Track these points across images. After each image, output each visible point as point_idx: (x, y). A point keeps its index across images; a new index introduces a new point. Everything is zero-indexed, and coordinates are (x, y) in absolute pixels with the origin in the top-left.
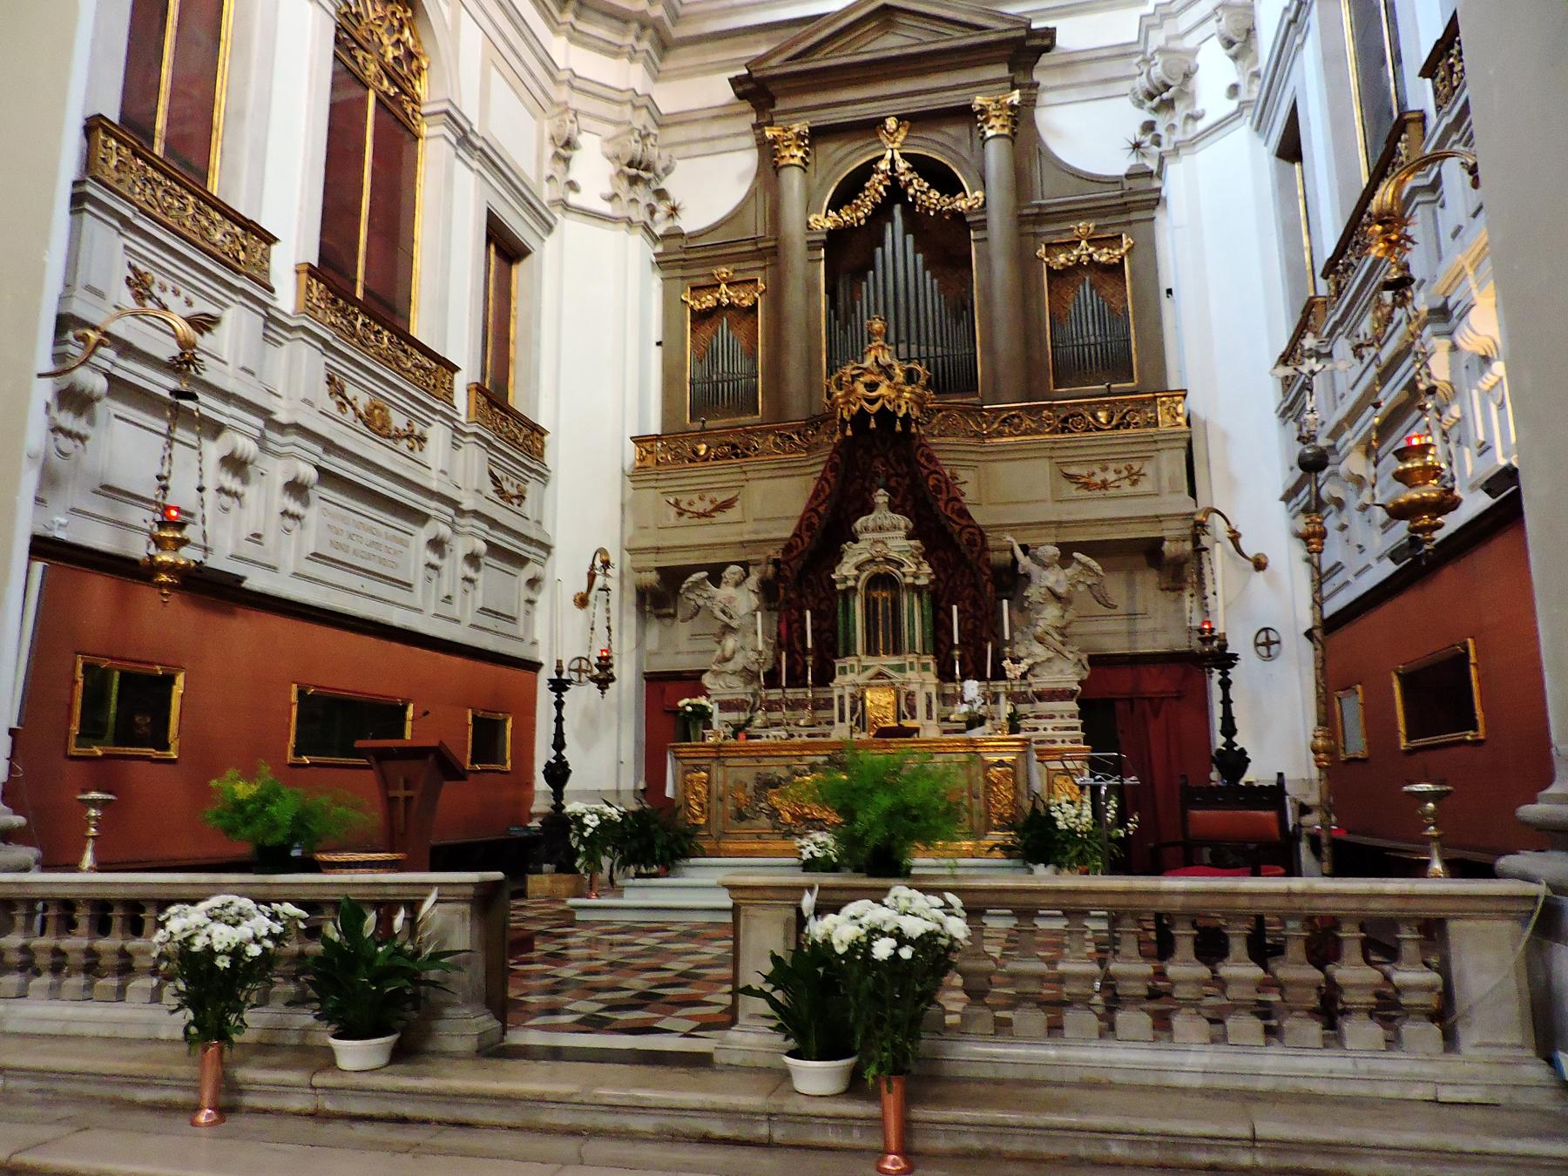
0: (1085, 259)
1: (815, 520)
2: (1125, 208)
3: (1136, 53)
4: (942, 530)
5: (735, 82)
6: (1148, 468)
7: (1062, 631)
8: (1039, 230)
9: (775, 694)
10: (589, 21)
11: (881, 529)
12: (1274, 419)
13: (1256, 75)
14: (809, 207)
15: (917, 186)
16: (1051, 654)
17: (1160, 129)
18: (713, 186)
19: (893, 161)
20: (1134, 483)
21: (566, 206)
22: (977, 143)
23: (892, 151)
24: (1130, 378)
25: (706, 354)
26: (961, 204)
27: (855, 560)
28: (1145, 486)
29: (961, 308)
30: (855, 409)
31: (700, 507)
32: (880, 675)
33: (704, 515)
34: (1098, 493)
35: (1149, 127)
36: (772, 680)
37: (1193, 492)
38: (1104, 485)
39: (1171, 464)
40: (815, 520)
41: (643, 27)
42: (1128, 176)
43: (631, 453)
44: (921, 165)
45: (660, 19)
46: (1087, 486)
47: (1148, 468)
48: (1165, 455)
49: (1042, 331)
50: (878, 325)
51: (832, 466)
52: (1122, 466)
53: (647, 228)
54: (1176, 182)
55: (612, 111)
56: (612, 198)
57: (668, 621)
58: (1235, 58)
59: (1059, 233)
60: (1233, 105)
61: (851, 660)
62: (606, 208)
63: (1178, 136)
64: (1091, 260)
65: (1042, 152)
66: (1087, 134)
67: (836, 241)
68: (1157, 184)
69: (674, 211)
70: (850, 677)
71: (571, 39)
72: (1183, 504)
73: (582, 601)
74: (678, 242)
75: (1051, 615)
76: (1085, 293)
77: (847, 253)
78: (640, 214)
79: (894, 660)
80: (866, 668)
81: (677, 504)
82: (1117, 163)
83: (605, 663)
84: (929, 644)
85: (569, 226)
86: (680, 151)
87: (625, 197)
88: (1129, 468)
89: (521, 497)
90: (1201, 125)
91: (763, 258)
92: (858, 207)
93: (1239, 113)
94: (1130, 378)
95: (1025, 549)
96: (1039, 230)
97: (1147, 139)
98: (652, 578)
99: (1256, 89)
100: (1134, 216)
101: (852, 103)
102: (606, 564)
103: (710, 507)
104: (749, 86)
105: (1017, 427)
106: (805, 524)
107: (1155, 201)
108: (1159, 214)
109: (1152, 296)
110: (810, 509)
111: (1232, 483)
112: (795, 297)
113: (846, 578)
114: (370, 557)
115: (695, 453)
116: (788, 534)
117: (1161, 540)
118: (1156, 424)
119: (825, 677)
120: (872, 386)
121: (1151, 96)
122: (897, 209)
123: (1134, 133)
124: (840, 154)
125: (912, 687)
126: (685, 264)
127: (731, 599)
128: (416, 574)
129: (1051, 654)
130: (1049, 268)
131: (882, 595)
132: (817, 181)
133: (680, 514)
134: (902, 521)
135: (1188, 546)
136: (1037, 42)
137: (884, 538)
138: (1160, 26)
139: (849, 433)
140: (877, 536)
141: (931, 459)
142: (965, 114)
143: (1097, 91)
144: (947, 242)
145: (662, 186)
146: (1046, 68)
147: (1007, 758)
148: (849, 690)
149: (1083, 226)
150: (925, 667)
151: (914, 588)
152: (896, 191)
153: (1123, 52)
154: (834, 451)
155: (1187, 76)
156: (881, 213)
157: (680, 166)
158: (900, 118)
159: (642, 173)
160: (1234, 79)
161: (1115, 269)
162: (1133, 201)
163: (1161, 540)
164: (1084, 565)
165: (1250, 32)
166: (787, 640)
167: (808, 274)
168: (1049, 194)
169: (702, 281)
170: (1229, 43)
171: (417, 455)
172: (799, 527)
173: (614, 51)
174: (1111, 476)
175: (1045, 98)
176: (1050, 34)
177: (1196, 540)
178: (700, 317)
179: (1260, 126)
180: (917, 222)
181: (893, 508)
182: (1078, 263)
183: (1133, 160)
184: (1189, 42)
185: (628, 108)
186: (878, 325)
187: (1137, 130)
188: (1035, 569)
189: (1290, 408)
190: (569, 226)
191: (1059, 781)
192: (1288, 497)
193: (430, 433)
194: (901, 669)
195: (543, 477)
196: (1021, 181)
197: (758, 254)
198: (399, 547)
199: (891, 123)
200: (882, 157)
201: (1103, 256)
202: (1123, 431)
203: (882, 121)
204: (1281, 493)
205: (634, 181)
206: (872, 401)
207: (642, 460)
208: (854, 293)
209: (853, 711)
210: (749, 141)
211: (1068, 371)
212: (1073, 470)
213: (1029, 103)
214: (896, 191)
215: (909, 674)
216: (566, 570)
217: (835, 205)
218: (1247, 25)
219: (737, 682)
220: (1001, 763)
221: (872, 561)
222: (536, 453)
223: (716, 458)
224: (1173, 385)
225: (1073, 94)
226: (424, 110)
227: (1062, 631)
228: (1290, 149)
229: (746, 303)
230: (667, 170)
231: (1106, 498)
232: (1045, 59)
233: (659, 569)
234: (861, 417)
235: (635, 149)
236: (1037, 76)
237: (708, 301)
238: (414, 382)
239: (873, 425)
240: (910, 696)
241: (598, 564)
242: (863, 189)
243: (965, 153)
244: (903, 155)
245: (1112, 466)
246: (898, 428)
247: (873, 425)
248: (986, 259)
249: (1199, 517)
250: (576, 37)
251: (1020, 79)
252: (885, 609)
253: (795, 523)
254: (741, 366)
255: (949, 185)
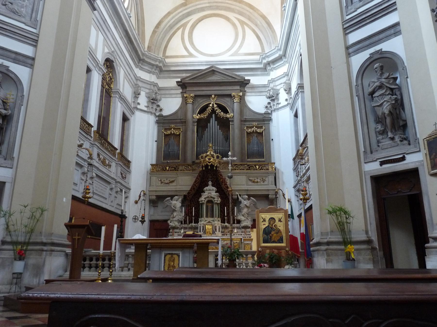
0: (255, 131)
1: (195, 187)
2: (264, 121)
3: (267, 87)
4: (223, 191)
5: (177, 82)
6: (267, 179)
7: (248, 214)
8: (245, 123)
9: (186, 226)
10: (144, 65)
11: (210, 190)
12: (292, 171)
13: (291, 98)
14: (193, 113)
15: (218, 111)
16: (245, 219)
17: (272, 105)
18: (171, 105)
19: (213, 105)
20: (264, 182)
21: (137, 109)
22: (232, 103)
23: (213, 102)
24: (264, 158)
25: (167, 145)
26: (228, 116)
27: (204, 197)
28: (266, 183)
29: (227, 138)
30: (205, 164)
31: (166, 182)
32: (209, 222)
33: (167, 183)
34: (256, 184)
35: (269, 103)
36: (185, 222)
37: (276, 185)
38: (257, 182)
39: (271, 178)
40: (195, 187)
41: (157, 67)
42: (264, 114)
43: (150, 167)
44: (220, 106)
45: (161, 66)
46: (254, 182)
47: (267, 179)
48: (270, 177)
49: (245, 146)
50: (211, 145)
51: (199, 175)
52: (261, 178)
53: (155, 114)
54: (274, 116)
55: (148, 87)
56: (147, 107)
57: (156, 208)
58: (287, 93)
59: (249, 124)
60: (286, 103)
61: (202, 219)
62: (146, 109)
63: (275, 107)
64: (256, 131)
65: (246, 106)
66: (256, 103)
67: (199, 120)
68: (270, 116)
69: (161, 110)
70: (202, 222)
71: (140, 69)
72: (273, 187)
73: (136, 202)
74: (162, 118)
75: (245, 210)
76: (254, 139)
77: (202, 125)
78: (154, 111)
79: (212, 219)
80: (206, 221)
81: (161, 180)
82: (262, 110)
83: (143, 217)
84: (219, 215)
85: (137, 113)
86: (163, 96)
87: (151, 107)
88: (263, 179)
89: (125, 178)
90: (280, 106)
91: (182, 123)
92: (205, 114)
93: (288, 104)
94: (264, 158)
95: (240, 195)
96: (245, 123)
97: (269, 106)
98: (154, 197)
99: (291, 100)
100: (266, 122)
101: (205, 91)
102: (145, 194)
103: (169, 182)
104: (181, 84)
105: (239, 168)
106: (193, 188)
107: (270, 120)
108: (270, 122)
109: (269, 140)
110: (194, 185)
111: (284, 183)
112: (189, 134)
113: (202, 201)
114: (99, 192)
115: (166, 169)
116: (189, 189)
117: (269, 195)
118: (268, 170)
119: (197, 222)
120: (210, 159)
121: (270, 98)
122: (214, 115)
123: (266, 104)
124: (201, 101)
125: (216, 225)
126: (163, 123)
127: (175, 204)
128: (107, 196)
129: (245, 219)
130: (247, 132)
131: (210, 205)
132: (196, 107)
133: (162, 183)
134: (215, 189)
135: (274, 196)
136: (246, 82)
137: (210, 192)
138: (272, 83)
139: (204, 169)
140: (209, 192)
141: (221, 175)
142: (230, 96)
143: (259, 94)
144: (225, 124)
145: (158, 104)
146: (248, 87)
147: (238, 242)
148: (202, 225)
149: (255, 124)
150: (219, 221)
151: (216, 203)
152: (213, 111)
153: (264, 86)
154: (200, 172)
155: (278, 94)
156: (210, 116)
157: (163, 99)
158: (215, 95)
159: (155, 102)
160: (287, 98)
161: (261, 134)
162: (265, 119)
163: (269, 195)
164: (253, 200)
165: (290, 89)
166: (188, 213)
167: (193, 129)
168: (247, 116)
169: (167, 127)
170: (286, 91)
171: (110, 169)
172: (191, 188)
173: (150, 72)
174: (259, 180)
175: (248, 94)
176: (249, 81)
177: (276, 195)
178: (166, 136)
179: (291, 109)
180: (218, 118)
181: (213, 185)
182: (253, 131)
183: (266, 110)
184: (278, 88)
185: (152, 86)
186: (211, 145)
187: (267, 104)
188: (242, 200)
189: (295, 169)
190: (137, 113)
191: (246, 246)
192: (295, 187)
193: (112, 164)
194: (213, 221)
195: (130, 172)
196: (241, 112)
197: (182, 122)
198: (104, 190)
199: (213, 96)
200: (211, 103)
201: (259, 131)
202: (261, 171)
203: (211, 95)
204: (293, 186)
205: (153, 103)
206: (209, 162)
207: (153, 170)
208: (203, 133)
209: (203, 230)
210: (180, 95)
211: (250, 155)
212: (251, 178)
213: (244, 95)
214: (213, 111)
215: (215, 222)
216: (134, 195)
217: (200, 113)
218: (290, 87)
219: (177, 223)
220: (237, 243)
221: (208, 197)
222: (129, 167)
223: (171, 170)
224: (273, 161)
225: (253, 94)
226: (113, 91)
227: (248, 214)
228: (296, 116)
229: (178, 133)
230: (160, 100)
231: (257, 185)
232: (247, 86)
233: (156, 196)
234: (207, 166)
235: (154, 96)
236: (246, 89)
237: (169, 132)
238: (110, 153)
239: (209, 168)
240: (216, 227)
241: (142, 194)
242: (206, 110)
243: (229, 104)
244: (215, 103)
245: (259, 178)
246: (215, 168)
247: (209, 168)
248: (233, 129)
249: (276, 190)
250: (142, 69)
251: (242, 89)
252: (210, 208)
253: (191, 187)
254: (176, 148)
255: (226, 111)
